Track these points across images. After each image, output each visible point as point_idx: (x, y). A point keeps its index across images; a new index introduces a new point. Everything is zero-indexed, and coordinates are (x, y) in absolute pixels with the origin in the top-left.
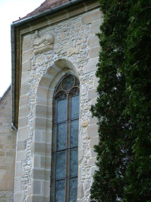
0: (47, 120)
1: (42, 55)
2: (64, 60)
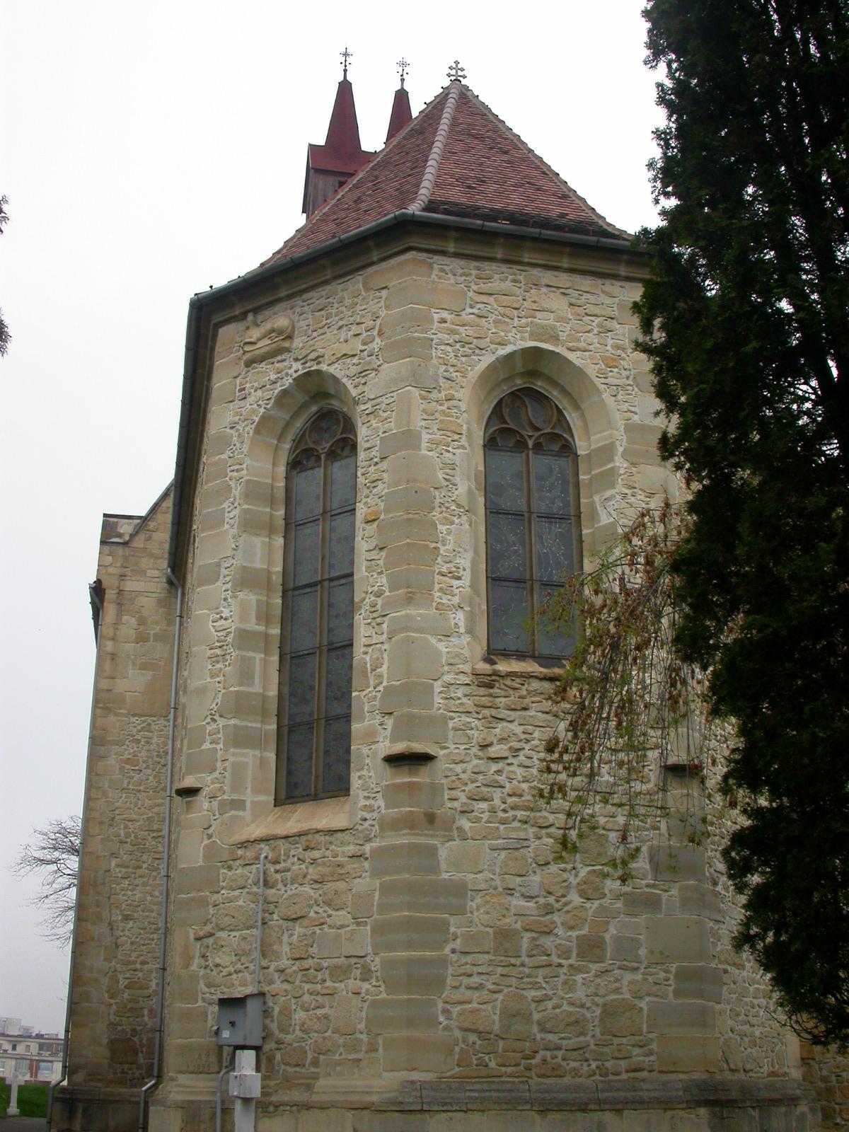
0: (271, 515)
1: (263, 365)
2: (319, 372)
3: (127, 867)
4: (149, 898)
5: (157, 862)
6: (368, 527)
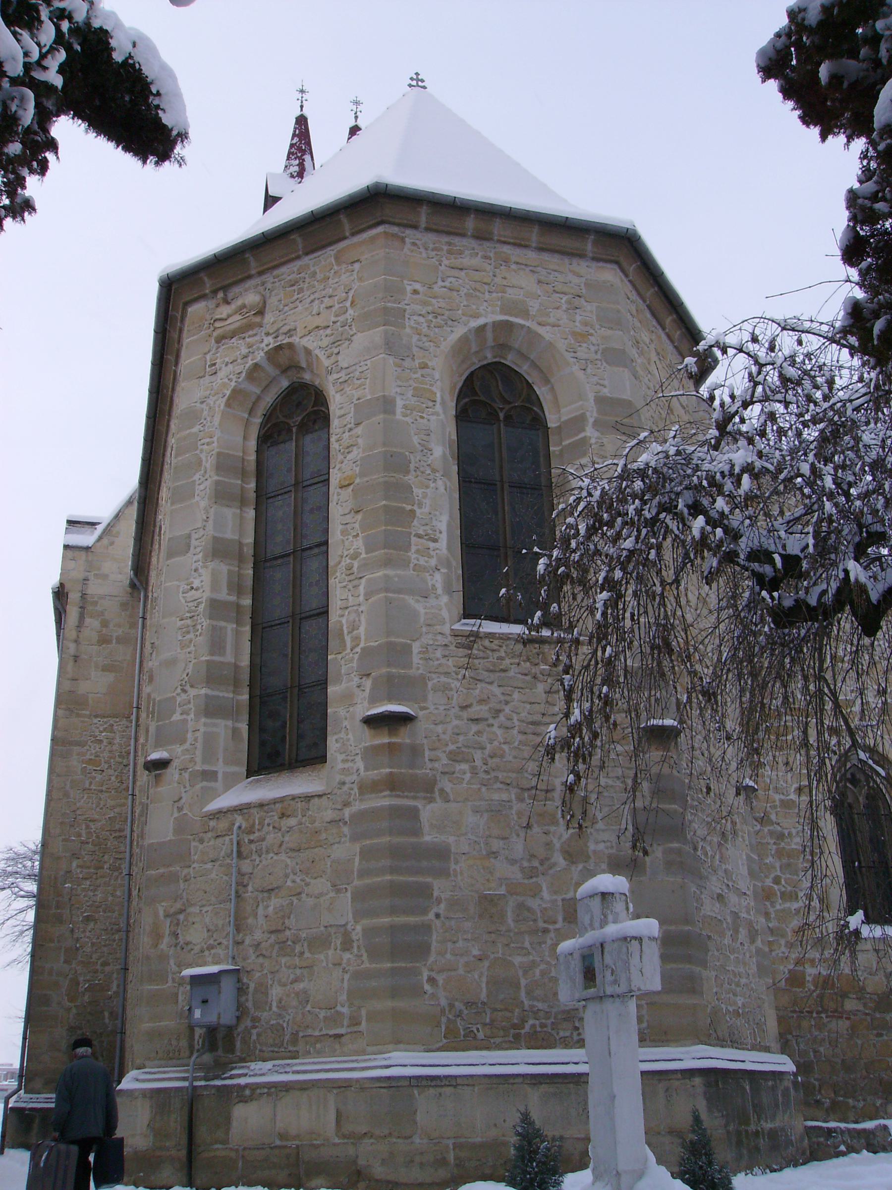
2: (290, 346)
3: (89, 868)
4: (110, 898)
5: (119, 862)
6: (342, 492)
